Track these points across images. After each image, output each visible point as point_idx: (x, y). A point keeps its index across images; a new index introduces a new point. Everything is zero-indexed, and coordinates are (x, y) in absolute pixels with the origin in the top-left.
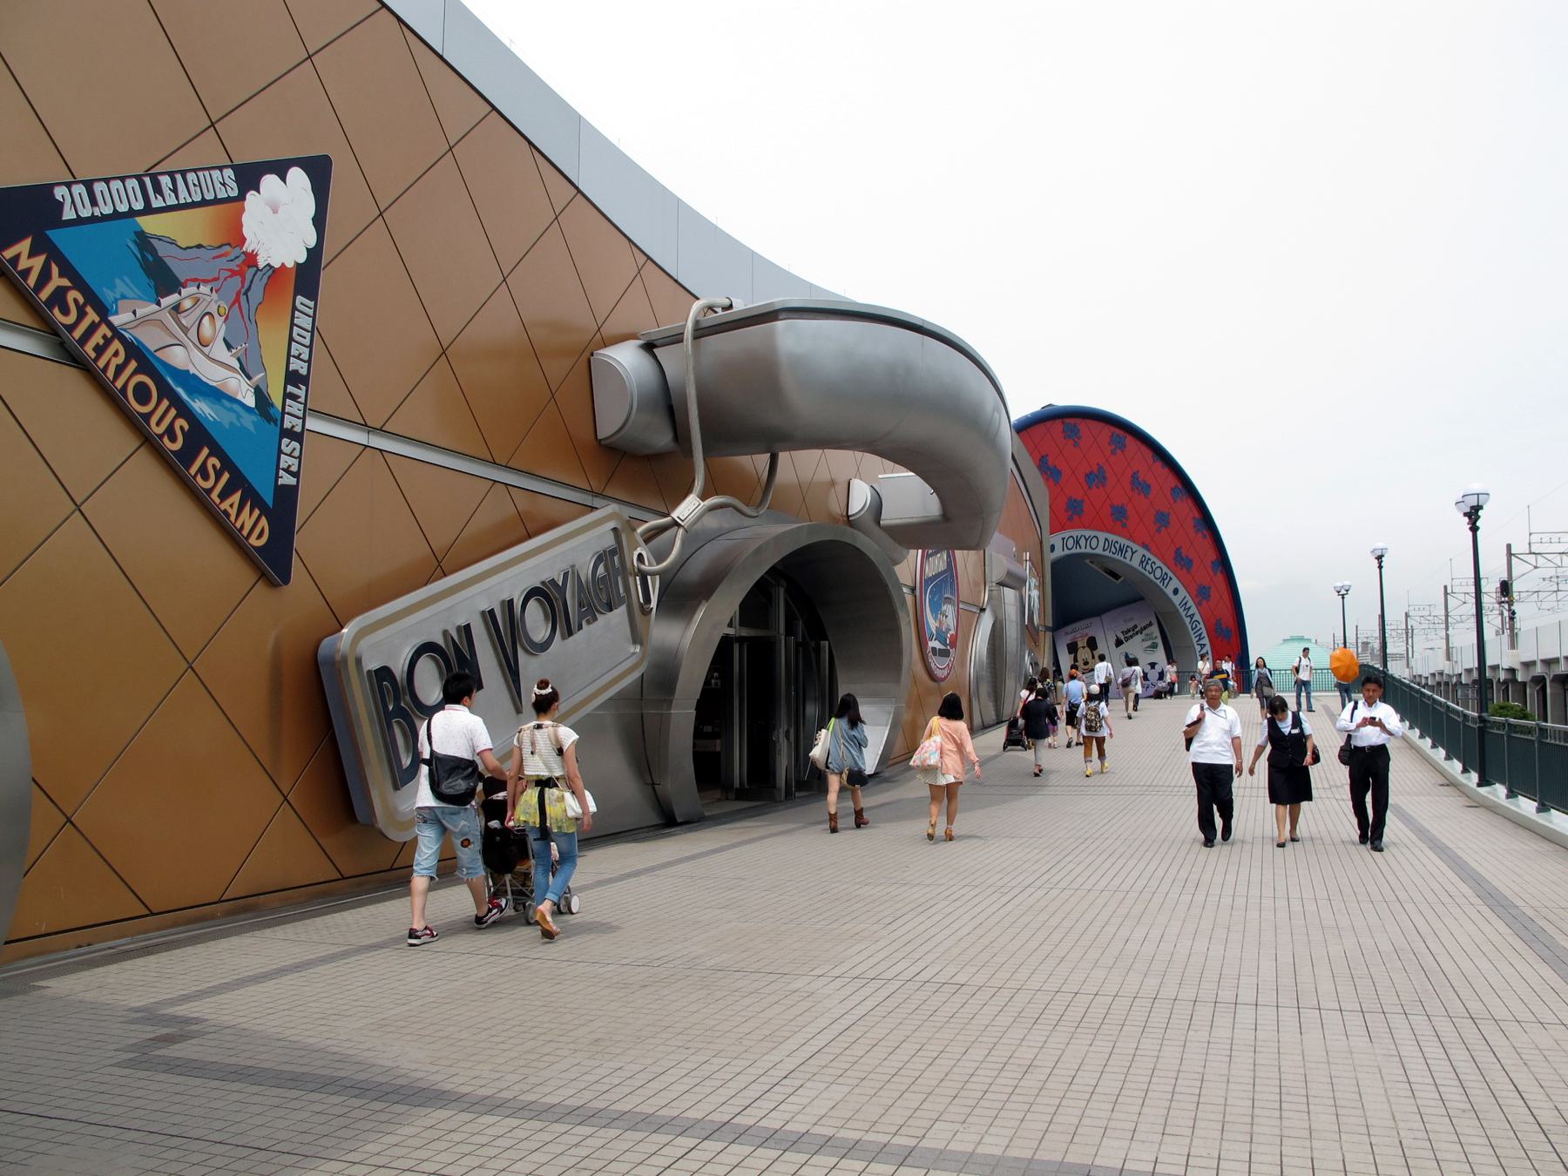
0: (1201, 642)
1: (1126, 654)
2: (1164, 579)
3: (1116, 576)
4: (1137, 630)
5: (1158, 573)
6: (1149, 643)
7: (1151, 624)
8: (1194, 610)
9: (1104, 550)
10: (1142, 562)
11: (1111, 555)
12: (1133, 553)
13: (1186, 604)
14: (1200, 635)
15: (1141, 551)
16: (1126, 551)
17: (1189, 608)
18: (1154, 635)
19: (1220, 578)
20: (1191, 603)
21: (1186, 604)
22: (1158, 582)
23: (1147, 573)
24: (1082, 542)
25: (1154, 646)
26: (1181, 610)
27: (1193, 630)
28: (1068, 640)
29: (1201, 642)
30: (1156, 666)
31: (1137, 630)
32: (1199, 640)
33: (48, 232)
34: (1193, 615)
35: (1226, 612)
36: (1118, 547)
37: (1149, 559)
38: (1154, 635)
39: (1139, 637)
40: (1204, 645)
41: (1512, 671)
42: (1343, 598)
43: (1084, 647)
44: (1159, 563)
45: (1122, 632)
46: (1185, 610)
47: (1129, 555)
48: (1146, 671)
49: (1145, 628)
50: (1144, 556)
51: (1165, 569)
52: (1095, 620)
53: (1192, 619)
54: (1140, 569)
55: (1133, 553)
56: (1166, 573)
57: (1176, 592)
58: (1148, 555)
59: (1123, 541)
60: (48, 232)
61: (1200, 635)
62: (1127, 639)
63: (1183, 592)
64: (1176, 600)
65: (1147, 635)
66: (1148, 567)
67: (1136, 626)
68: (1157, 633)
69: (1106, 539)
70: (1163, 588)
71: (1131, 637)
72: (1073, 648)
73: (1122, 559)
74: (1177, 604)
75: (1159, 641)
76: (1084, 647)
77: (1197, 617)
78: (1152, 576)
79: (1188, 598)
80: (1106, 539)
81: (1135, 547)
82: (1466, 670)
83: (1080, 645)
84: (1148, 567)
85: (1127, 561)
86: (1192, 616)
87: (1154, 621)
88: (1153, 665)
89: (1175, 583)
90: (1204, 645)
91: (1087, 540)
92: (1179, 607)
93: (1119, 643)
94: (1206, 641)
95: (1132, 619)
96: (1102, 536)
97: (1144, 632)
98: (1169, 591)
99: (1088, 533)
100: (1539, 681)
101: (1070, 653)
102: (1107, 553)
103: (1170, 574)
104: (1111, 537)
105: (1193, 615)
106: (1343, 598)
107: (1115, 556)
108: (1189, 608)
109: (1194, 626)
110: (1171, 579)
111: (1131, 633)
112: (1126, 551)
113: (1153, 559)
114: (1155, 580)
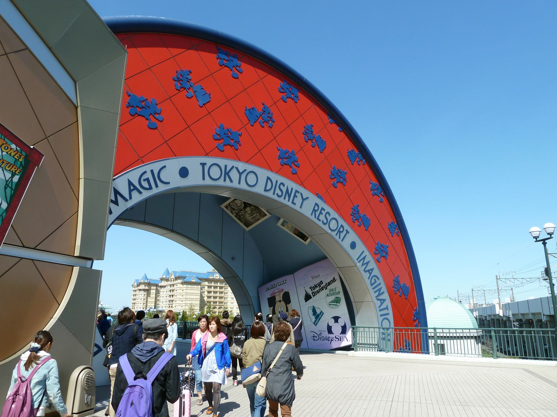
0: (380, 297)
1: (314, 307)
2: (340, 232)
3: (304, 237)
4: (322, 286)
5: (333, 225)
6: (332, 298)
7: (334, 280)
8: (373, 265)
9: (265, 190)
10: (314, 210)
11: (275, 197)
12: (303, 200)
13: (364, 258)
14: (379, 290)
15: (313, 199)
16: (295, 196)
17: (367, 263)
18: (337, 291)
19: (397, 240)
20: (369, 258)
21: (364, 258)
22: (334, 234)
23: (320, 224)
24: (234, 175)
25: (337, 301)
26: (359, 265)
27: (372, 285)
28: (268, 295)
29: (380, 297)
30: (339, 320)
31: (322, 286)
32: (379, 295)
33: (114, 200)
34: (372, 270)
35: (405, 281)
36: (284, 190)
37: (322, 209)
38: (337, 291)
39: (324, 293)
40: (384, 300)
41: (486, 317)
42: (544, 244)
43: (280, 301)
44: (334, 214)
45: (310, 288)
46: (363, 264)
47: (298, 200)
48: (330, 325)
49: (329, 284)
50: (316, 204)
51: (341, 222)
52: (289, 278)
53: (370, 274)
54: (312, 218)
55: (303, 200)
56: (342, 226)
57: (353, 246)
58: (322, 204)
59: (291, 184)
60: (114, 200)
61: (379, 290)
62: (314, 294)
63: (361, 247)
64: (355, 254)
65: (331, 290)
66: (322, 217)
67: (321, 282)
68: (340, 289)
69: (268, 178)
70: (340, 241)
71: (318, 292)
72: (272, 302)
73: (290, 204)
74: (355, 258)
75: (342, 296)
76: (280, 301)
77: (376, 272)
78: (326, 228)
79: (367, 253)
80: (268, 178)
81: (306, 193)
82: (489, 315)
83: (278, 299)
84: (322, 217)
85: (297, 207)
86: (370, 271)
87: (337, 278)
88: (336, 319)
89: (352, 236)
90: (384, 300)
91: (240, 174)
92: (357, 261)
93: (308, 298)
94: (386, 296)
95: (318, 276)
96: (263, 173)
97: (329, 287)
98: (346, 244)
99: (242, 166)
100: (493, 320)
101: (270, 306)
102: (270, 194)
103: (347, 227)
104: (275, 177)
105: (372, 270)
106: (544, 244)
107: (281, 200)
108: (367, 263)
109: (373, 281)
110: (348, 232)
111: (317, 289)
112: (295, 196)
113: (328, 209)
114: (329, 231)
